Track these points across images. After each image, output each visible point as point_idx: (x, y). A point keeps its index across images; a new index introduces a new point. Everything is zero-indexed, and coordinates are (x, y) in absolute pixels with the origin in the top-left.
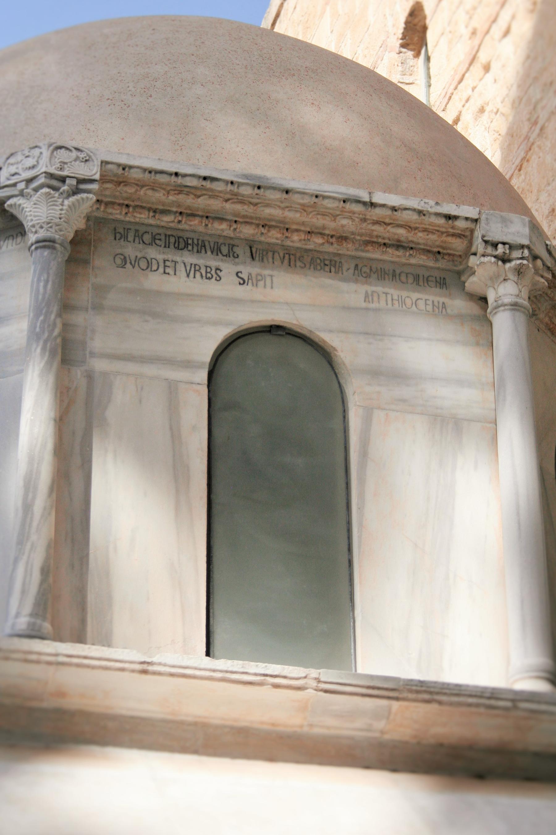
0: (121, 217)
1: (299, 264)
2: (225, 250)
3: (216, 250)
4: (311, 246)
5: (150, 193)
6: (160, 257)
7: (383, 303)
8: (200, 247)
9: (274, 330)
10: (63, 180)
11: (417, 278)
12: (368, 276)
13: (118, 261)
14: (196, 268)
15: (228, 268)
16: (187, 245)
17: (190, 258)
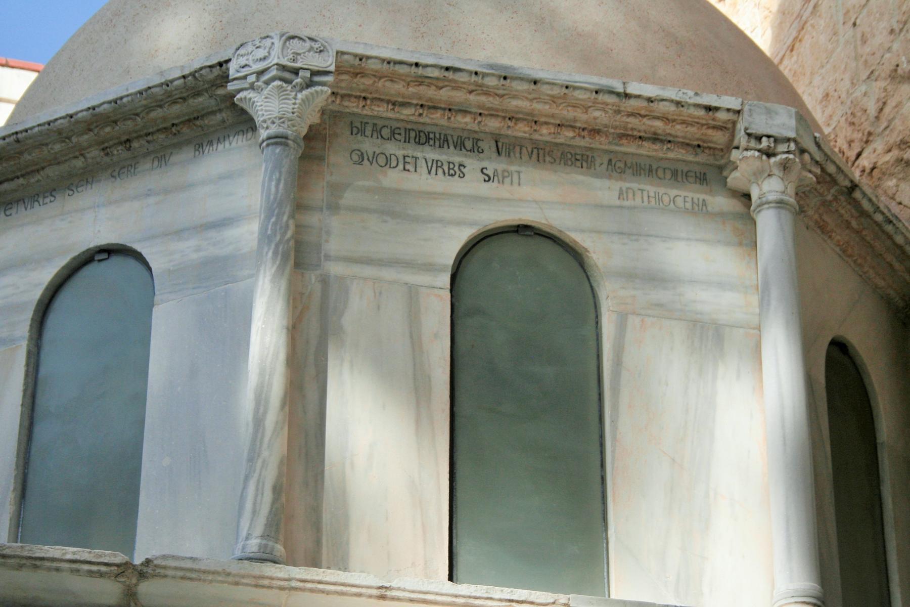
0: (358, 111)
1: (548, 159)
2: (469, 144)
3: (460, 145)
4: (561, 140)
5: (388, 84)
6: (400, 153)
7: (638, 200)
8: (443, 141)
9: (522, 230)
10: (296, 72)
11: (675, 173)
12: (623, 172)
13: (355, 157)
14: (438, 164)
15: (472, 164)
16: (428, 139)
17: (431, 154)
